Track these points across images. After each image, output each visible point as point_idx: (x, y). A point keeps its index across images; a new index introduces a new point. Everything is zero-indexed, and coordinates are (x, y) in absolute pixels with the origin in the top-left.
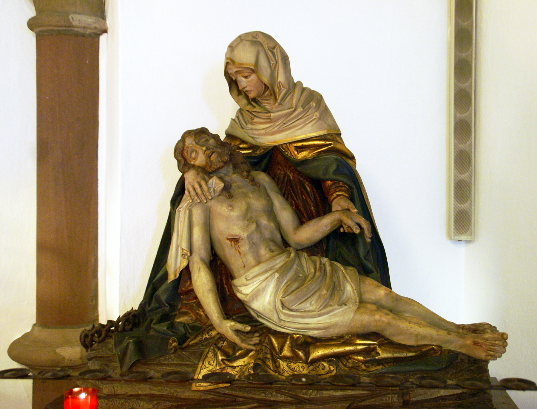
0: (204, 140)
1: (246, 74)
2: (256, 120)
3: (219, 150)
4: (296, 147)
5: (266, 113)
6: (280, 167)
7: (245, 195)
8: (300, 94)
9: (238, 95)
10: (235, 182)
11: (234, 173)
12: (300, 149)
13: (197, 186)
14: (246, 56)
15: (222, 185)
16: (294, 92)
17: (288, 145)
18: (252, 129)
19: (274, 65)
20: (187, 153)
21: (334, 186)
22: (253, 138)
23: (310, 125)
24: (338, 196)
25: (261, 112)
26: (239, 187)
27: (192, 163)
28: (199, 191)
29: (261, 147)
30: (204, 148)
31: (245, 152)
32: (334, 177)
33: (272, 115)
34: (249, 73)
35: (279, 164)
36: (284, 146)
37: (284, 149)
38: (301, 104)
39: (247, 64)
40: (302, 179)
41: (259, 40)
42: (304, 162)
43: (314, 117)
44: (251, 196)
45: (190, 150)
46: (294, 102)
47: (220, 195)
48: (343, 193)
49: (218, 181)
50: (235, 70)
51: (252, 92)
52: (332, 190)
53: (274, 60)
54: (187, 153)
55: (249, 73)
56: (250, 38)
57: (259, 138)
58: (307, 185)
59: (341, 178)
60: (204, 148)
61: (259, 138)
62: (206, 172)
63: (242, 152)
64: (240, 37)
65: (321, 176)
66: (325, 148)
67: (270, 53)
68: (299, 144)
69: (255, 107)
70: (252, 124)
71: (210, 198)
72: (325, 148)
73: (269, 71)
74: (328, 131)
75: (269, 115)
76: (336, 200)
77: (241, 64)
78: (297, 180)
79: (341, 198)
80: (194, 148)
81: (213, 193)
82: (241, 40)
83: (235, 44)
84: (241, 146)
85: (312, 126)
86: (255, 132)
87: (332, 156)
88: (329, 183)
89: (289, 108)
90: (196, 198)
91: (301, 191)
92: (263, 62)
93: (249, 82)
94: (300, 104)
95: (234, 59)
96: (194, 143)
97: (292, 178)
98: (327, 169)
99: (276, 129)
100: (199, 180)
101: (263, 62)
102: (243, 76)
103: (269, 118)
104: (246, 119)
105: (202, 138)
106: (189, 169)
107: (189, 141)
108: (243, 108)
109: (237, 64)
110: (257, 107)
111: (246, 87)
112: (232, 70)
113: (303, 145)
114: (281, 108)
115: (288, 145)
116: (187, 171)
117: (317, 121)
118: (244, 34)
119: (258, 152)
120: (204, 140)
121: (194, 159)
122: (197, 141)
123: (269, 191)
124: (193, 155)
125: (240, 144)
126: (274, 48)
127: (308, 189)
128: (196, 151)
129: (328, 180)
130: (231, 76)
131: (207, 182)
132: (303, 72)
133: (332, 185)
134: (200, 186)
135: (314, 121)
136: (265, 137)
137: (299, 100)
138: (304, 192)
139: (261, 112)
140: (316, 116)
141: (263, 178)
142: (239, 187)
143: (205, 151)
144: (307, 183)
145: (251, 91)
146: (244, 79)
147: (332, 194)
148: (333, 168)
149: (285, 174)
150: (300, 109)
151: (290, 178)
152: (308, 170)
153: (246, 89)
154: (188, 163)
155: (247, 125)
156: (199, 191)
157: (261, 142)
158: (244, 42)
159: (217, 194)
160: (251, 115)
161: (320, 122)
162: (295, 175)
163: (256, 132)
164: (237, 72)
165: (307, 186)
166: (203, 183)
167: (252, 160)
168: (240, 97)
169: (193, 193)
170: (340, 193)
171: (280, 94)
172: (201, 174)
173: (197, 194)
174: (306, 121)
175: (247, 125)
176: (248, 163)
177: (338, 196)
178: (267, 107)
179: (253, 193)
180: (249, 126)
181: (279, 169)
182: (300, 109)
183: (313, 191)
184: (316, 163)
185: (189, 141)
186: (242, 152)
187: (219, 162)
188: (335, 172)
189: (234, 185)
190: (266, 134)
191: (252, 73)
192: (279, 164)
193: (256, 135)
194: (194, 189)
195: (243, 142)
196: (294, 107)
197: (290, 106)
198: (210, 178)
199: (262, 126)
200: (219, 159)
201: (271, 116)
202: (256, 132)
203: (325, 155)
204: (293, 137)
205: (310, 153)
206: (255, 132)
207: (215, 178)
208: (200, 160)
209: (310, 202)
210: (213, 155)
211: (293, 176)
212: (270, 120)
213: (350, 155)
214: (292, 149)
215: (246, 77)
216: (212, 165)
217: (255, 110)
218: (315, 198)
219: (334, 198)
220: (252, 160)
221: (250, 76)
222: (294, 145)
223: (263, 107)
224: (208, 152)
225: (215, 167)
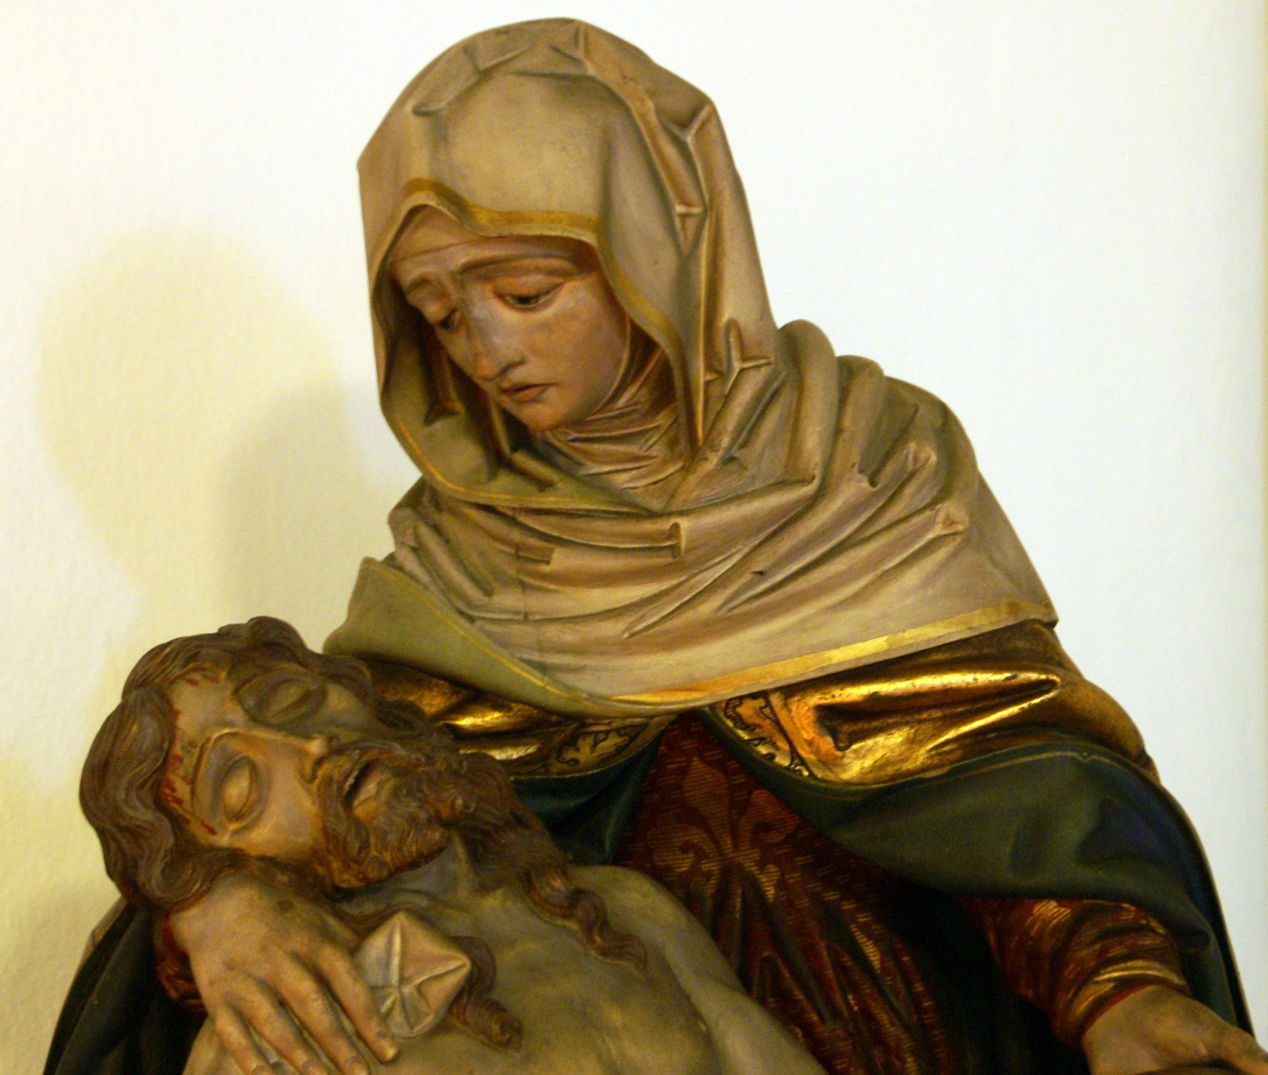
0: (290, 695)
1: (529, 283)
2: (561, 560)
3: (399, 751)
4: (831, 717)
5: (628, 516)
6: (696, 836)
7: (584, 1021)
8: (834, 396)
9: (429, 420)
10: (512, 943)
11: (484, 889)
12: (848, 723)
13: (300, 985)
14: (534, 168)
15: (456, 967)
16: (800, 388)
17: (776, 700)
18: (526, 617)
19: (691, 223)
20: (192, 781)
21: (1089, 932)
22: (543, 668)
23: (912, 577)
24: (1125, 986)
25: (588, 515)
26: (535, 971)
27: (224, 840)
28: (316, 1011)
29: (598, 719)
30: (315, 747)
31: (514, 754)
32: (1088, 876)
33: (685, 524)
34: (552, 272)
35: (690, 816)
36: (746, 710)
37: (747, 727)
38: (856, 458)
39: (550, 216)
40: (831, 896)
41: (591, 71)
42: (892, 795)
43: (937, 531)
44: (616, 1017)
45: (211, 762)
46: (813, 440)
47: (441, 1028)
48: (1154, 970)
49: (426, 944)
50: (463, 256)
51: (552, 393)
52: (1084, 954)
53: (693, 196)
54: (192, 781)
55: (552, 272)
56: (539, 59)
57: (579, 670)
58: (864, 928)
59: (1125, 880)
60: (315, 747)
61: (579, 670)
62: (331, 889)
63: (498, 755)
64: (468, 49)
65: (1009, 878)
66: (1014, 710)
67: (670, 151)
68: (855, 693)
69: (544, 485)
70: (524, 586)
71: (390, 1052)
72: (1014, 710)
73: (668, 259)
74: (1014, 607)
75: (666, 525)
76: (1116, 1012)
77: (513, 218)
78: (806, 903)
79: (1153, 1000)
80: (236, 745)
81: (398, 1017)
82: (485, 75)
83: (449, 96)
84: (466, 722)
85: (927, 582)
86: (553, 633)
87: (1064, 754)
88: (1050, 911)
89: (781, 484)
90: (301, 1057)
91: (841, 969)
92: (636, 206)
93: (546, 327)
94: (852, 452)
95: (461, 189)
96: (236, 715)
97: (771, 892)
98: (1036, 832)
99: (706, 609)
100: (300, 941)
101: (636, 206)
102: (500, 296)
103: (668, 545)
104: (475, 560)
105: (275, 687)
106: (212, 880)
107: (199, 707)
108: (448, 485)
109: (483, 218)
110: (563, 485)
111: (521, 363)
112: (440, 254)
113: (875, 697)
114: (736, 483)
115: (776, 700)
116: (199, 896)
117: (954, 554)
118: (485, 35)
119: (585, 753)
120: (290, 695)
121: (237, 816)
122: (251, 702)
123: (688, 980)
124: (237, 790)
125: (461, 708)
126: (685, 125)
127: (873, 954)
128: (253, 768)
129: (1041, 895)
130: (415, 298)
131: (353, 951)
132: (833, 260)
133: (1071, 930)
134: (324, 983)
135: (941, 554)
136: (623, 662)
137: (838, 431)
138: (857, 975)
139: (588, 515)
140: (949, 522)
141: (638, 900)
142: (535, 971)
143: (319, 762)
144: (862, 918)
145: (545, 386)
146: (509, 316)
147: (1086, 977)
148: (1075, 824)
149: (729, 873)
150: (853, 488)
151: (761, 894)
152: (915, 846)
153: (518, 375)
154: (193, 841)
155: (489, 593)
156: (316, 1011)
157: (601, 689)
158: (504, 83)
159: (429, 1020)
160: (516, 535)
161: (969, 557)
162: (794, 878)
163: (569, 636)
164: (470, 269)
165: (861, 938)
166: (336, 964)
167: (551, 804)
168: (439, 425)
169: (274, 1027)
170: (1138, 968)
171: (727, 399)
172: (303, 908)
173: (303, 1031)
174: (885, 554)
175: (489, 593)
176: (538, 825)
177: (1125, 986)
178: (622, 480)
179: (619, 998)
180: (509, 600)
181: (685, 848)
182: (853, 488)
183: (899, 964)
184: (964, 803)
185: (199, 707)
186: (498, 755)
187: (413, 820)
188: (1090, 850)
189: (506, 959)
190: (635, 643)
191: (567, 275)
192: (690, 816)
193: (563, 649)
194: (282, 1004)
195: (473, 694)
196: (818, 473)
197: (779, 473)
198: (366, 928)
199: (601, 598)
200: (413, 807)
201: (676, 526)
202: (569, 636)
203: (1013, 755)
204: (814, 649)
205: (912, 742)
206: (553, 633)
207: (399, 921)
208: (284, 816)
209: (891, 1029)
210: (370, 788)
211: (781, 885)
212: (672, 557)
213: (1130, 746)
214: (801, 716)
215: (525, 301)
216: (365, 846)
217: (548, 501)
218: (915, 999)
219: (1100, 1005)
220: (551, 804)
221: (551, 290)
222: (816, 699)
223: (594, 484)
224: (340, 767)
225: (383, 855)
